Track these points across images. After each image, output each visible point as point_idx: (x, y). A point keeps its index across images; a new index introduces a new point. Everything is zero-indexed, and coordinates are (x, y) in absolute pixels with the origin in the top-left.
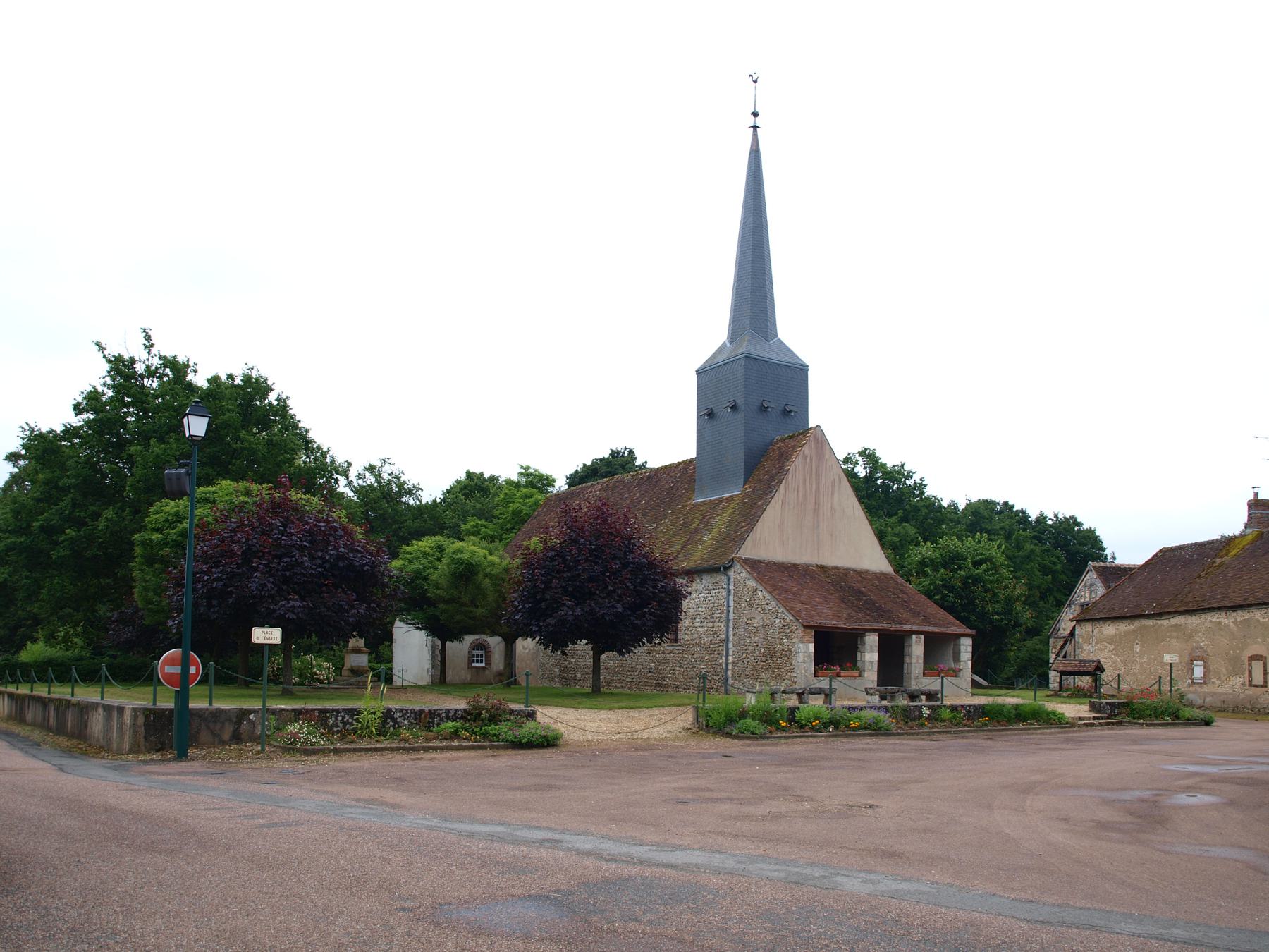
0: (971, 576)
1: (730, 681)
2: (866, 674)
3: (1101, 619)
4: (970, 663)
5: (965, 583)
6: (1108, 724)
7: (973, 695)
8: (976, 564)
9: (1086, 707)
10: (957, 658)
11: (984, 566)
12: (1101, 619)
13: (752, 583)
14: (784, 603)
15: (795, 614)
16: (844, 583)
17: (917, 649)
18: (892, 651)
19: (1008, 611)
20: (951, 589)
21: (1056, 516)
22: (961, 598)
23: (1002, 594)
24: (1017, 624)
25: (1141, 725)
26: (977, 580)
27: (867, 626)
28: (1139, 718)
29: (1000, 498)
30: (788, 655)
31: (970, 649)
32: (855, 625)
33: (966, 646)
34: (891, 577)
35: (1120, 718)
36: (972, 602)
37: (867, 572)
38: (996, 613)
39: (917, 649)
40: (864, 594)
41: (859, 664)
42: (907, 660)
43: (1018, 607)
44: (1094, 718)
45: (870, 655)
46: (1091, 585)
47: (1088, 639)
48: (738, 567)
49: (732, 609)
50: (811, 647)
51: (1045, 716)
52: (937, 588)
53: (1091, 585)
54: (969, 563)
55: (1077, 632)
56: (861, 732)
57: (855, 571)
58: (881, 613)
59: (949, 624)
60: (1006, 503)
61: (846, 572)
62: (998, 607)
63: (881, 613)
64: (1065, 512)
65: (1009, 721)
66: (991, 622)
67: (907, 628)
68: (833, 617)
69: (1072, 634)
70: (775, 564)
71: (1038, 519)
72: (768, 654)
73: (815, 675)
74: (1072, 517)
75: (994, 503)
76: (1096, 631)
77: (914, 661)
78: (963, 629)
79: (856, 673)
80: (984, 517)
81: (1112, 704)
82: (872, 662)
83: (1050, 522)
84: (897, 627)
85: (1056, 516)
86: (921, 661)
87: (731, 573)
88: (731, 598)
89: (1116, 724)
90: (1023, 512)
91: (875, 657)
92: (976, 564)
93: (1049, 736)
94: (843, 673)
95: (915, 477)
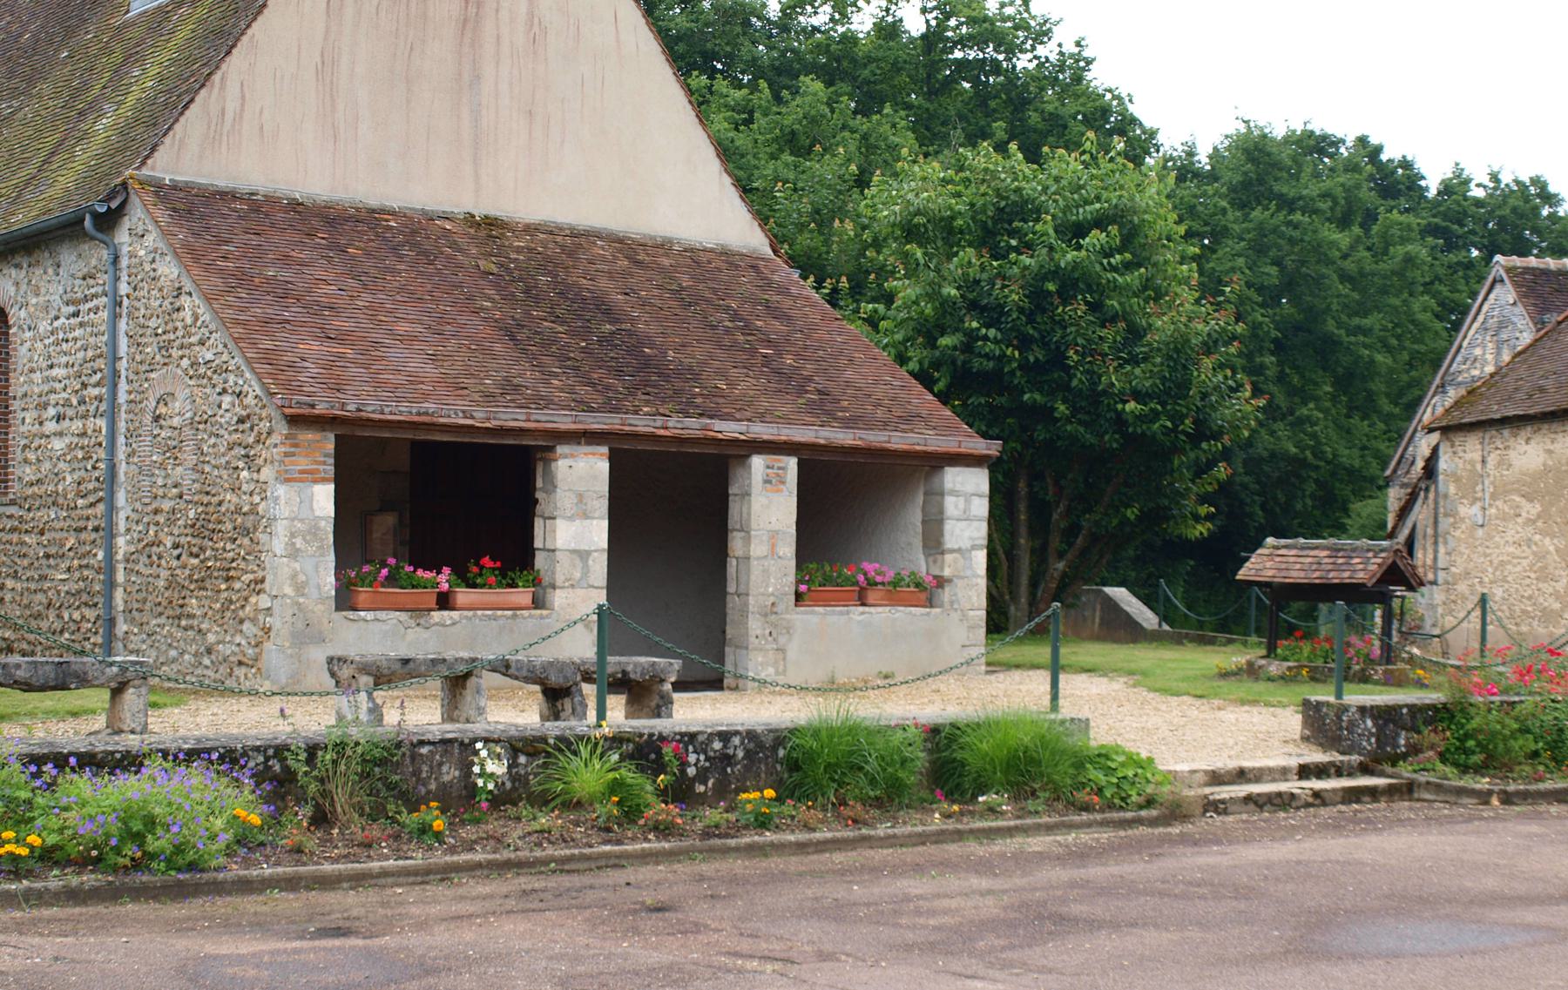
0: (1055, 273)
1: (122, 627)
2: (559, 598)
3: (1504, 422)
4: (981, 558)
5: (1038, 299)
6: (1353, 795)
7: (994, 666)
8: (1075, 232)
9: (1293, 722)
10: (933, 542)
11: (1095, 238)
12: (1504, 422)
13: (169, 270)
14: (245, 333)
15: (273, 367)
16: (551, 286)
17: (768, 507)
18: (673, 513)
19: (1175, 386)
20: (993, 314)
21: (1495, 177)
22: (1024, 343)
23: (1162, 326)
24: (1203, 431)
25: (1484, 797)
26: (1071, 283)
27: (564, 421)
28: (1479, 770)
29: (1344, 126)
30: (249, 526)
31: (981, 507)
32: (512, 417)
33: (966, 498)
34: (753, 263)
35: (1405, 771)
36: (1057, 359)
37: (664, 246)
38: (1137, 396)
39: (768, 507)
40: (609, 313)
41: (540, 561)
42: (736, 544)
43: (1206, 372)
44: (1304, 772)
45: (576, 520)
46: (1502, 325)
47: (1471, 485)
48: (137, 215)
49: (122, 365)
50: (323, 498)
51: (1063, 774)
52: (946, 307)
53: (1502, 325)
54: (1046, 226)
55: (1443, 464)
56: (54, 880)
57: (619, 242)
58: (647, 373)
59: (910, 419)
60: (1362, 141)
61: (577, 242)
62: (1141, 376)
63: (647, 373)
64: (1517, 169)
65: (890, 796)
66: (1120, 421)
67: (729, 429)
68: (433, 383)
69: (1430, 470)
70: (295, 205)
71: (1447, 189)
72: (203, 529)
73: (345, 600)
74: (1536, 181)
75: (1397, 182)
76: (1492, 459)
77: (758, 549)
78: (939, 429)
79: (522, 595)
80: (1277, 165)
81: (1387, 716)
82: (583, 555)
83: (1479, 193)
84: (691, 426)
85: (1495, 177)
86: (788, 549)
87: (122, 237)
88: (123, 325)
89: (1391, 792)
90: (1406, 164)
91: (597, 533)
92: (1075, 232)
93: (1042, 856)
94: (463, 595)
95: (1059, 34)
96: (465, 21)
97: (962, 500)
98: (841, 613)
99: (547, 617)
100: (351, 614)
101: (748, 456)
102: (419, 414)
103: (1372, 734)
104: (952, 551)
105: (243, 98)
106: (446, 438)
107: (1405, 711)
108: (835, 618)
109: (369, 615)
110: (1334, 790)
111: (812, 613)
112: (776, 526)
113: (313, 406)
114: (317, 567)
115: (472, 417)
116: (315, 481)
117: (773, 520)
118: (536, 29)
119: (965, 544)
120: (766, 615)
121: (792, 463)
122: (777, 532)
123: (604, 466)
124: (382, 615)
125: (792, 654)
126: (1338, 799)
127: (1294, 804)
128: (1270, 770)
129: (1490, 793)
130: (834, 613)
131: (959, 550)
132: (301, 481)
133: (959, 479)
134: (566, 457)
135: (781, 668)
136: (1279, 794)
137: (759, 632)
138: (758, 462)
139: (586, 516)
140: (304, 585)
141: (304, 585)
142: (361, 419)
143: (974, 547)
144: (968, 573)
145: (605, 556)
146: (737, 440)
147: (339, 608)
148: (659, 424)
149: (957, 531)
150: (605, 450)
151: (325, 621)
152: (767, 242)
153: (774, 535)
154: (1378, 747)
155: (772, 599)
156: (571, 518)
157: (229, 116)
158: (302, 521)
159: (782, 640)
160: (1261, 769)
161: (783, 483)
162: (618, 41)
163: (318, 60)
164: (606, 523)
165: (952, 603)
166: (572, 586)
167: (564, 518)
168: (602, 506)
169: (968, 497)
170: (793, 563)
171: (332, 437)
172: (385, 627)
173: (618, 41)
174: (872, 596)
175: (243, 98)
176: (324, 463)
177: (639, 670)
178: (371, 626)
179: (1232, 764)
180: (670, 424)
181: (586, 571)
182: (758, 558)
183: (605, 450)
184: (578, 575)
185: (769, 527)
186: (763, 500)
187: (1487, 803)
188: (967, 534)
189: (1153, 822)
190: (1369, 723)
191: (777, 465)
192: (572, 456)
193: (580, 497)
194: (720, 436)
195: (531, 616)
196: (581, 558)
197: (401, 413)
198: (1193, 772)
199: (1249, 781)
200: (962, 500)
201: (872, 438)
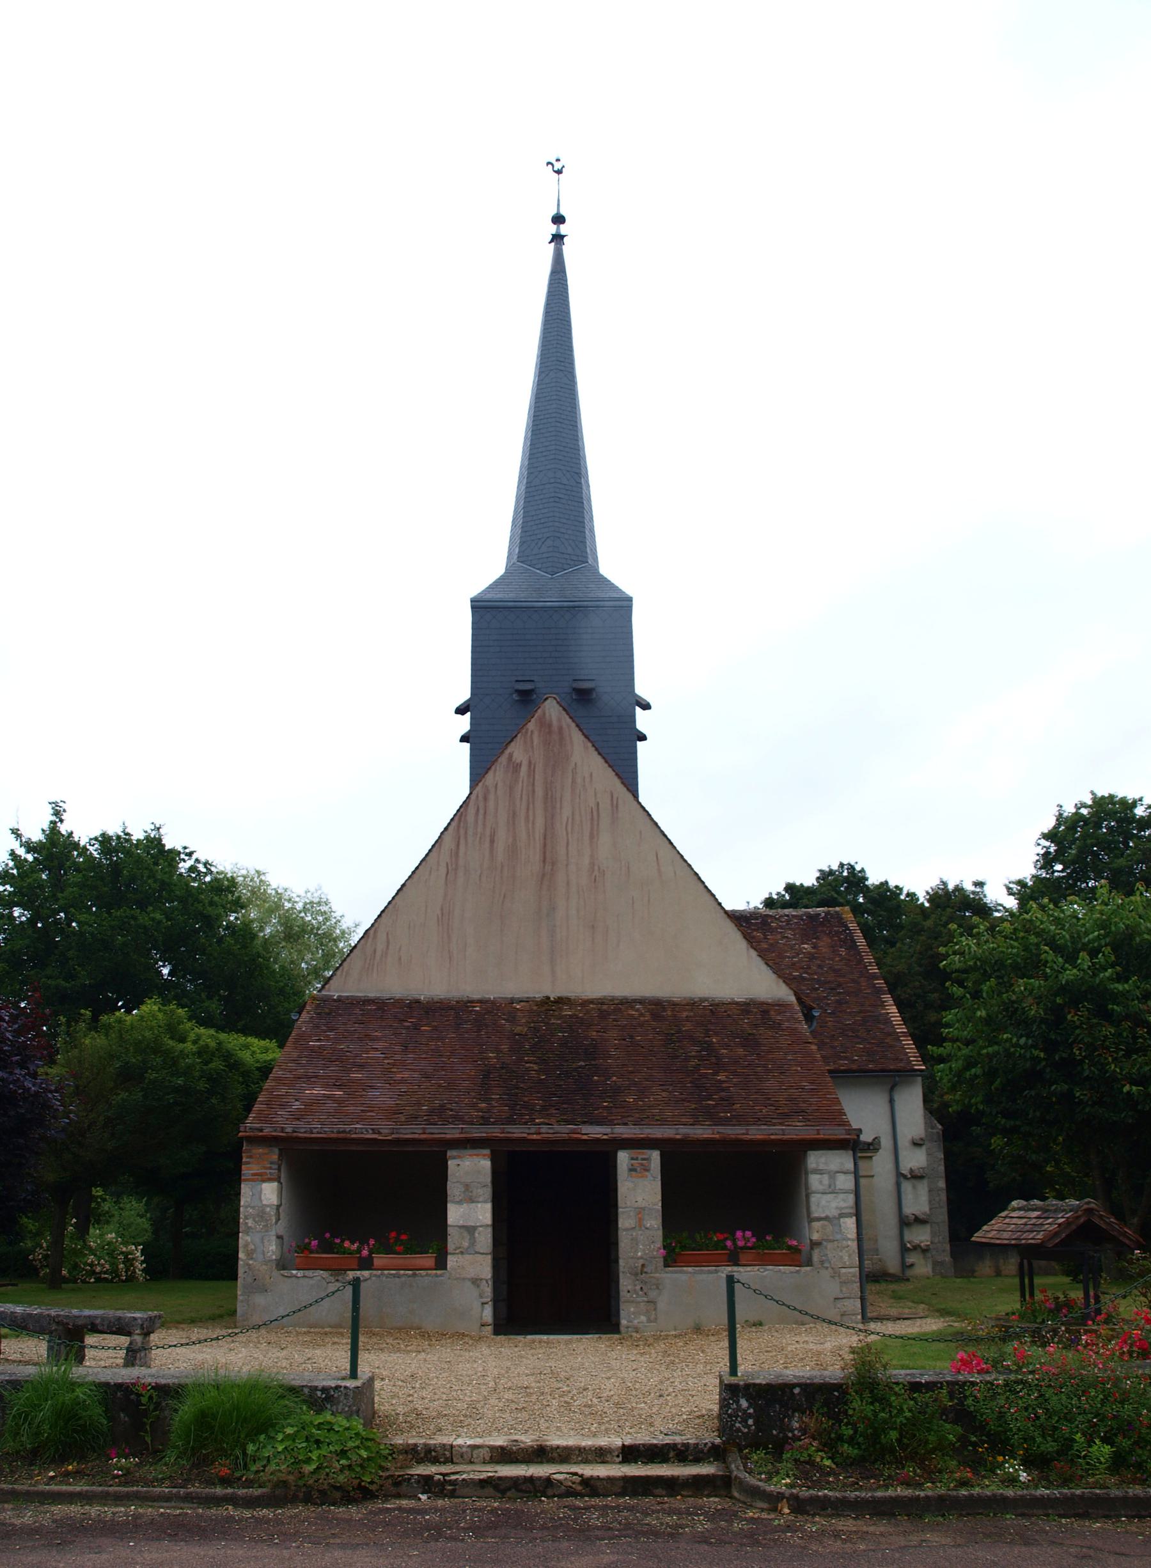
0: (1063, 989)
79: (428, 1260)
82: (471, 1230)
91: (483, 1213)
94: (379, 1260)
96: (544, 875)
97: (826, 1177)
98: (710, 1272)
99: (441, 1275)
100: (285, 1273)
101: (806, 1152)
102: (339, 1132)
103: (750, 1416)
104: (819, 1219)
105: (388, 942)
106: (360, 1148)
107: (797, 1391)
108: (704, 1276)
109: (300, 1273)
110: (610, 1480)
111: (681, 1272)
112: (641, 1203)
113: (261, 1130)
114: (262, 1239)
115: (379, 1133)
116: (264, 1181)
117: (640, 1199)
118: (596, 873)
119: (832, 1212)
120: (636, 1274)
121: (655, 1156)
122: (643, 1209)
123: (486, 1164)
124: (309, 1273)
125: (661, 1305)
126: (617, 1489)
127: (550, 1492)
128: (581, 1450)
129: (780, 1496)
130: (702, 1272)
131: (826, 1218)
132: (253, 1180)
133: (823, 1160)
134: (454, 1158)
135: (653, 1317)
136: (531, 1479)
137: (629, 1288)
138: (815, 1159)
139: (472, 1200)
140: (253, 1251)
141: (253, 1251)
142: (297, 1138)
143: (842, 1215)
144: (838, 1237)
145: (490, 1230)
146: (598, 1140)
147: (666, 1265)
148: (532, 1131)
149: (823, 1203)
150: (487, 1152)
151: (267, 1277)
152: (791, 992)
153: (640, 1211)
154: (758, 1429)
155: (641, 1262)
156: (460, 1202)
157: (378, 954)
158: (253, 1208)
159: (653, 1294)
160: (568, 1449)
161: (648, 1170)
162: (659, 871)
163: (439, 912)
164: (489, 1206)
165: (822, 1262)
166: (462, 1253)
167: (453, 1202)
168: (487, 1192)
169: (833, 1175)
170: (660, 1233)
171: (276, 1151)
172: (311, 1282)
173: (659, 871)
174: (743, 1257)
175: (388, 942)
176: (270, 1168)
177: (106, 1323)
178: (302, 1281)
179: (528, 1440)
180: (543, 1131)
181: (473, 1242)
182: (626, 1230)
183: (487, 1152)
184: (466, 1244)
185: (636, 1205)
186: (629, 1184)
187: (774, 1509)
188: (834, 1205)
189: (251, 1503)
190: (744, 1403)
191: (640, 1157)
192: (459, 1157)
193: (467, 1187)
194: (585, 1137)
195: (427, 1275)
196: (469, 1232)
197: (325, 1132)
198: (474, 1447)
199: (551, 1461)
200: (826, 1177)
201: (730, 1132)
